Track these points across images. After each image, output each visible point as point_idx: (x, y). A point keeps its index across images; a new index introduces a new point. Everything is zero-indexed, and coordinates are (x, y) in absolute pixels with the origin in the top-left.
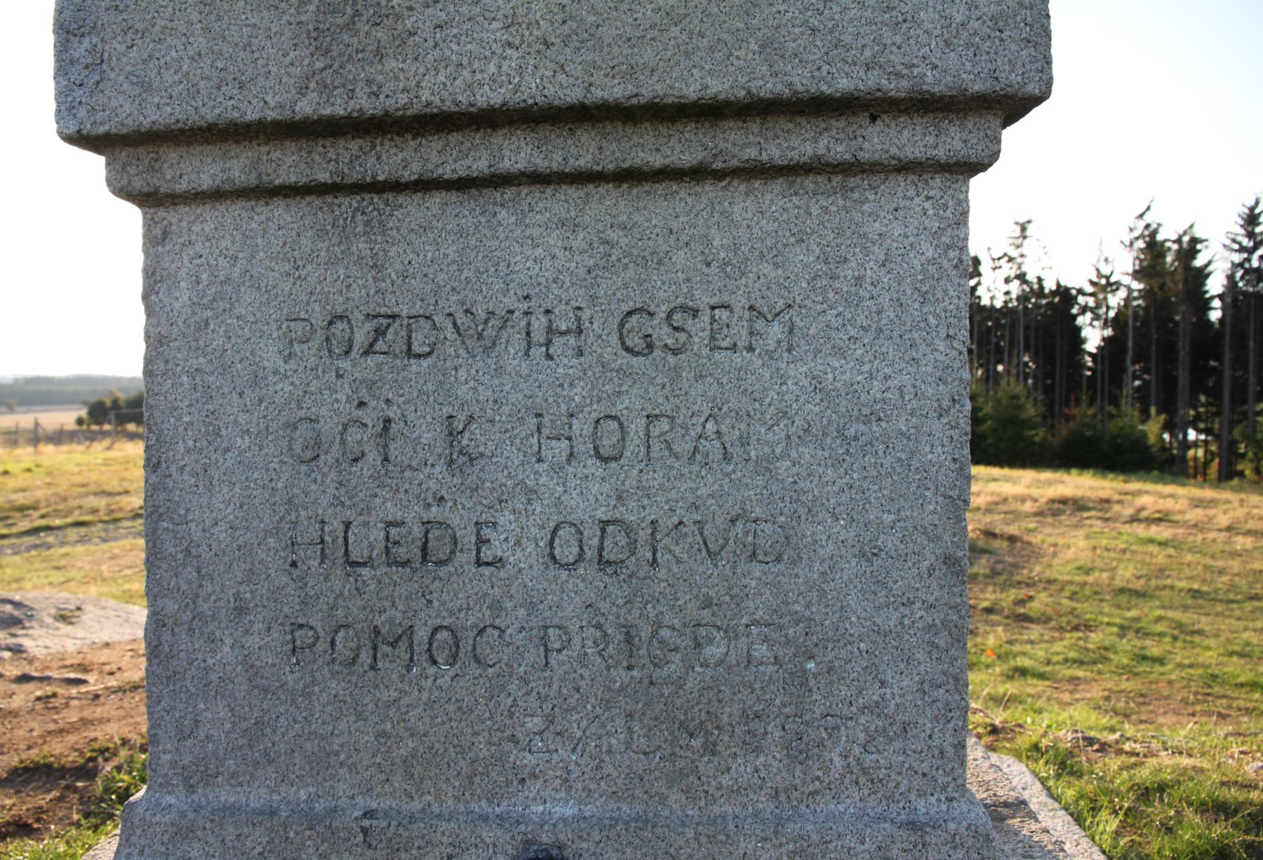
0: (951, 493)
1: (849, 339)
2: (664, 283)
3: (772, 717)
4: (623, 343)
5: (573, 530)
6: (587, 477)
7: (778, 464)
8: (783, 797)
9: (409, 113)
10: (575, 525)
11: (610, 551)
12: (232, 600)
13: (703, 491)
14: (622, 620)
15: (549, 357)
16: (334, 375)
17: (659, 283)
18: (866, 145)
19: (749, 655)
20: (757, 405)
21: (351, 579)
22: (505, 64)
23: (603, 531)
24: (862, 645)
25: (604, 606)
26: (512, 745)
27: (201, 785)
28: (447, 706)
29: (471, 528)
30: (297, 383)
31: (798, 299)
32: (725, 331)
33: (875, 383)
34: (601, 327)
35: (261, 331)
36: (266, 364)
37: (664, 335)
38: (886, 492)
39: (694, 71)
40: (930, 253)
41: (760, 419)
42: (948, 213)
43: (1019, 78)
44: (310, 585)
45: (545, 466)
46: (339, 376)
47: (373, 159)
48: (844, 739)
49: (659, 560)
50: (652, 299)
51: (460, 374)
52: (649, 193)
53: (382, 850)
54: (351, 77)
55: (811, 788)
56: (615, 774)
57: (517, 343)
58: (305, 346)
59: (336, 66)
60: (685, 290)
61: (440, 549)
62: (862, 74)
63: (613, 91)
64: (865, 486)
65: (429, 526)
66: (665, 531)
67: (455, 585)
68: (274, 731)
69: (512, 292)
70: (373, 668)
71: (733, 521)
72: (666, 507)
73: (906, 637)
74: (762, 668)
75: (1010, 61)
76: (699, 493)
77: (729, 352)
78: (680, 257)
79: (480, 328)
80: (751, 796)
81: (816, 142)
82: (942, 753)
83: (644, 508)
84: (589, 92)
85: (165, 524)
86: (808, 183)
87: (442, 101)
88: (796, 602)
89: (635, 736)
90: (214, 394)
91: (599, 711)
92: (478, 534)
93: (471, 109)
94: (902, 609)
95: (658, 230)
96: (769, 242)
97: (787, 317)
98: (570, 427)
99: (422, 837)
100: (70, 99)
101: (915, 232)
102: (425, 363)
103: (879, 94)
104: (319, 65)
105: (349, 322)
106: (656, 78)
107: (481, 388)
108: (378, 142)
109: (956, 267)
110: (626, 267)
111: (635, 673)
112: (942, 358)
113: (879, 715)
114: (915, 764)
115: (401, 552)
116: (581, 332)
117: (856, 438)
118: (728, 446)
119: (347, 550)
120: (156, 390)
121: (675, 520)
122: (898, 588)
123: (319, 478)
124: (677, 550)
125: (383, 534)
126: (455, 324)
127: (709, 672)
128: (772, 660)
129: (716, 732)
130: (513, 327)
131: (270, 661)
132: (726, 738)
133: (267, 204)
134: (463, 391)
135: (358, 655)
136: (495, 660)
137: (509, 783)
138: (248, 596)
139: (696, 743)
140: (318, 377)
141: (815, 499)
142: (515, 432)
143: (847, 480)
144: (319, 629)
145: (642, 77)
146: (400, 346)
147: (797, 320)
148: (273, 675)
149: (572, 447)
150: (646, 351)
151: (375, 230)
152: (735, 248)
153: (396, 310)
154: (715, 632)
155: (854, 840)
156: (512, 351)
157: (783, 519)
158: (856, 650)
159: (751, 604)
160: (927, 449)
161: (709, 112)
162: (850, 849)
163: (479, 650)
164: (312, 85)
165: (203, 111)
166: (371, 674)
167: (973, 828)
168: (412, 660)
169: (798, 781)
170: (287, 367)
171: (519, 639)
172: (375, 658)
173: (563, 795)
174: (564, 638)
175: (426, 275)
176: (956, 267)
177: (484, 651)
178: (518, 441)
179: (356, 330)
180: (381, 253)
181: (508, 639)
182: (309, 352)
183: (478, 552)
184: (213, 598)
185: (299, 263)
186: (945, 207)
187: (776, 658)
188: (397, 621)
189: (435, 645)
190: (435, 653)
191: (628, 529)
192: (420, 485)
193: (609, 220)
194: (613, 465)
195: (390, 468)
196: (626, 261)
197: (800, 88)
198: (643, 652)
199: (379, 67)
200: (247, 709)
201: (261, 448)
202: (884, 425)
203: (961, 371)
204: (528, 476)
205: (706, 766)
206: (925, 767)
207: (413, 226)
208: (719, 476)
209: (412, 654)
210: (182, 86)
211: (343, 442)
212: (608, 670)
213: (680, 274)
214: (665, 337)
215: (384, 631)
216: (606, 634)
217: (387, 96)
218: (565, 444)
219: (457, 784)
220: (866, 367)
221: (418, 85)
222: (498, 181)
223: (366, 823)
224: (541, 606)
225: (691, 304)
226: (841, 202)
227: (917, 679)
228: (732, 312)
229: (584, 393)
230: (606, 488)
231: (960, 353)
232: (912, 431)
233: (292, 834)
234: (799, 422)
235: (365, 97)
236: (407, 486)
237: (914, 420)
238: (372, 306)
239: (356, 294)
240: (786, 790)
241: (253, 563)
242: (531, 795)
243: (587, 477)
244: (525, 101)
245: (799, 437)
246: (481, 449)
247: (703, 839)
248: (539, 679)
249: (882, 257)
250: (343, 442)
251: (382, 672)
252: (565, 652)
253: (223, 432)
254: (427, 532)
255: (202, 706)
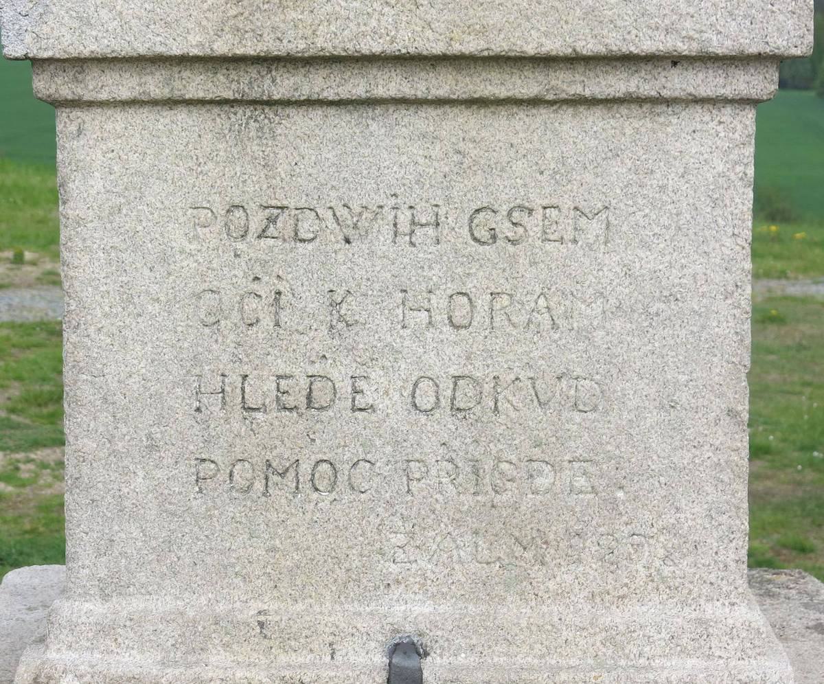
0: (734, 360)
1: (654, 235)
2: (505, 187)
3: (590, 535)
4: (472, 235)
5: (431, 383)
6: (442, 341)
7: (595, 334)
8: (598, 600)
9: (306, 55)
10: (432, 380)
11: (463, 400)
12: (144, 439)
13: (536, 354)
14: (470, 456)
15: (412, 244)
16: (232, 254)
17: (502, 187)
18: (669, 85)
19: (571, 485)
20: (579, 287)
21: (247, 422)
22: (383, 19)
23: (455, 384)
24: (661, 478)
25: (456, 444)
26: (380, 556)
27: (114, 594)
28: (326, 525)
29: (349, 382)
30: (201, 261)
31: (614, 202)
32: (554, 227)
33: (674, 271)
34: (455, 221)
35: (169, 216)
36: (174, 244)
37: (505, 229)
38: (681, 358)
39: (532, 32)
40: (720, 168)
41: (581, 298)
42: (737, 136)
43: (785, 43)
44: (212, 426)
45: (408, 331)
46: (237, 256)
47: (269, 82)
48: (647, 554)
49: (500, 408)
50: (496, 200)
51: (339, 257)
52: (494, 113)
53: (275, 639)
54: (259, 24)
55: (621, 593)
56: (463, 580)
57: (387, 231)
58: (207, 229)
59: (246, 14)
60: (523, 194)
61: (321, 397)
62: (662, 37)
63: (471, 45)
64: (664, 352)
65: (313, 379)
66: (505, 385)
67: (334, 427)
68: (180, 548)
69: (382, 191)
70: (265, 493)
71: (559, 378)
72: (506, 366)
73: (697, 473)
74: (581, 496)
75: (778, 29)
76: (532, 355)
77: (557, 243)
78: (519, 166)
79: (355, 219)
80: (573, 598)
81: (628, 81)
82: (726, 566)
83: (488, 366)
84: (451, 45)
85: (84, 377)
86: (624, 110)
87: (334, 47)
88: (608, 443)
89: (480, 549)
90: (127, 268)
91: (450, 529)
92: (353, 385)
93: (356, 54)
94: (694, 450)
95: (501, 144)
96: (590, 156)
97: (604, 216)
98: (429, 301)
99: (309, 629)
100: (17, 27)
101: (709, 150)
102: (310, 246)
103: (675, 53)
104: (233, 12)
105: (245, 210)
106: (502, 36)
107: (356, 269)
108: (273, 67)
109: (741, 179)
110: (475, 173)
111: (479, 498)
112: (728, 252)
113: (675, 535)
114: (703, 575)
115: (290, 401)
116: (438, 224)
117: (657, 314)
118: (555, 318)
119: (243, 398)
120: (76, 264)
121: (513, 377)
122: (690, 434)
123: (220, 339)
124: (514, 400)
125: (274, 385)
126: (334, 215)
127: (539, 497)
128: (590, 489)
129: (545, 546)
130: (382, 219)
131: (177, 489)
132: (552, 551)
133: (171, 109)
134: (342, 271)
135: (252, 484)
136: (367, 487)
137: (376, 588)
138: (159, 436)
139: (529, 555)
140: (219, 256)
141: (624, 362)
142: (385, 304)
143: (650, 347)
144: (220, 463)
145: (492, 36)
146: (289, 232)
147: (612, 219)
148: (179, 501)
149: (430, 317)
150: (491, 241)
151: (267, 135)
152: (563, 160)
153: (285, 203)
154: (544, 465)
155: (652, 630)
156: (382, 239)
157: (598, 377)
158: (657, 483)
159: (573, 444)
160: (715, 324)
161: (546, 61)
162: (649, 637)
163: (353, 480)
164: (227, 29)
165: (136, 45)
166: (264, 499)
167: (747, 624)
168: (297, 488)
169: (609, 587)
170: (192, 247)
171: (386, 471)
172: (267, 486)
173: (421, 597)
174: (423, 469)
175: (310, 175)
176: (741, 179)
177: (356, 482)
178: (387, 311)
179: (250, 218)
180: (272, 155)
181: (377, 470)
182: (211, 236)
183: (354, 400)
184: (127, 438)
185: (201, 160)
186: (734, 130)
187: (593, 487)
188: (286, 457)
189: (317, 476)
190: (317, 482)
191: (476, 382)
192: (306, 345)
193: (461, 135)
194: (463, 332)
195: (281, 332)
196: (475, 168)
197: (615, 48)
198: (487, 480)
199: (282, 17)
200: (157, 529)
201: (170, 313)
202: (680, 304)
203: (743, 263)
204: (394, 340)
205: (537, 572)
206: (712, 577)
207: (298, 133)
208: (548, 342)
209: (298, 483)
210: (116, 22)
211: (241, 310)
212: (459, 496)
213: (518, 180)
214: (506, 231)
215: (274, 464)
216: (457, 467)
217: (289, 41)
218: (424, 314)
219: (334, 589)
220: (668, 258)
221: (314, 32)
222: (371, 102)
223: (262, 618)
224: (405, 444)
225: (527, 204)
226: (649, 125)
227: (706, 506)
228: (560, 211)
229: (440, 274)
230: (458, 350)
231: (743, 248)
232: (703, 310)
233: (200, 629)
234: (613, 301)
235: (271, 41)
236: (294, 347)
237: (704, 301)
238: (265, 199)
239: (250, 189)
240: (601, 594)
241: (163, 408)
242: (395, 598)
243: (442, 341)
244: (400, 50)
245: (612, 313)
246: (357, 318)
247: (534, 628)
248: (402, 503)
249: (682, 170)
250: (241, 310)
251: (273, 498)
252: (423, 481)
253: (136, 300)
254: (311, 383)
255: (116, 528)
